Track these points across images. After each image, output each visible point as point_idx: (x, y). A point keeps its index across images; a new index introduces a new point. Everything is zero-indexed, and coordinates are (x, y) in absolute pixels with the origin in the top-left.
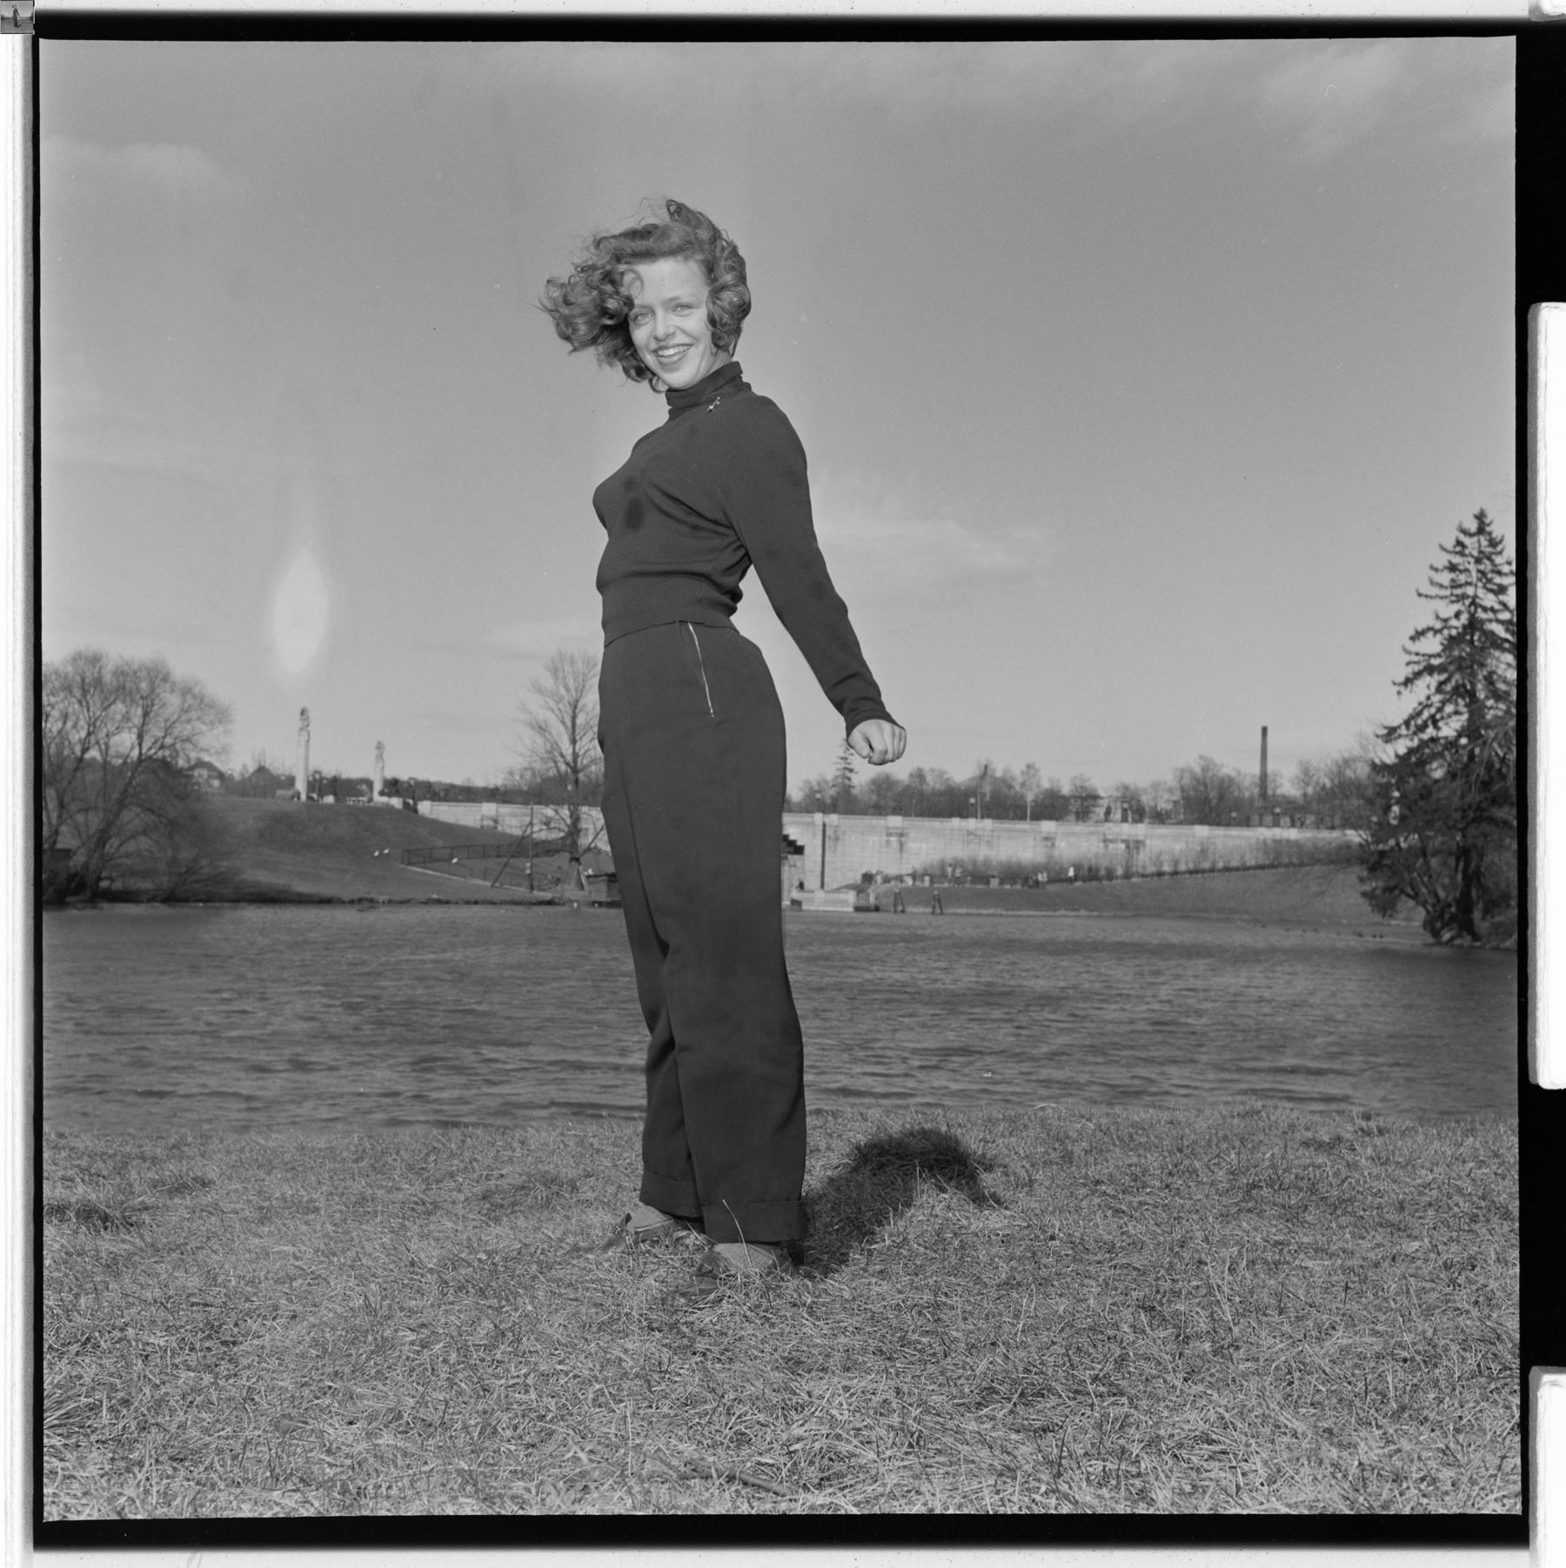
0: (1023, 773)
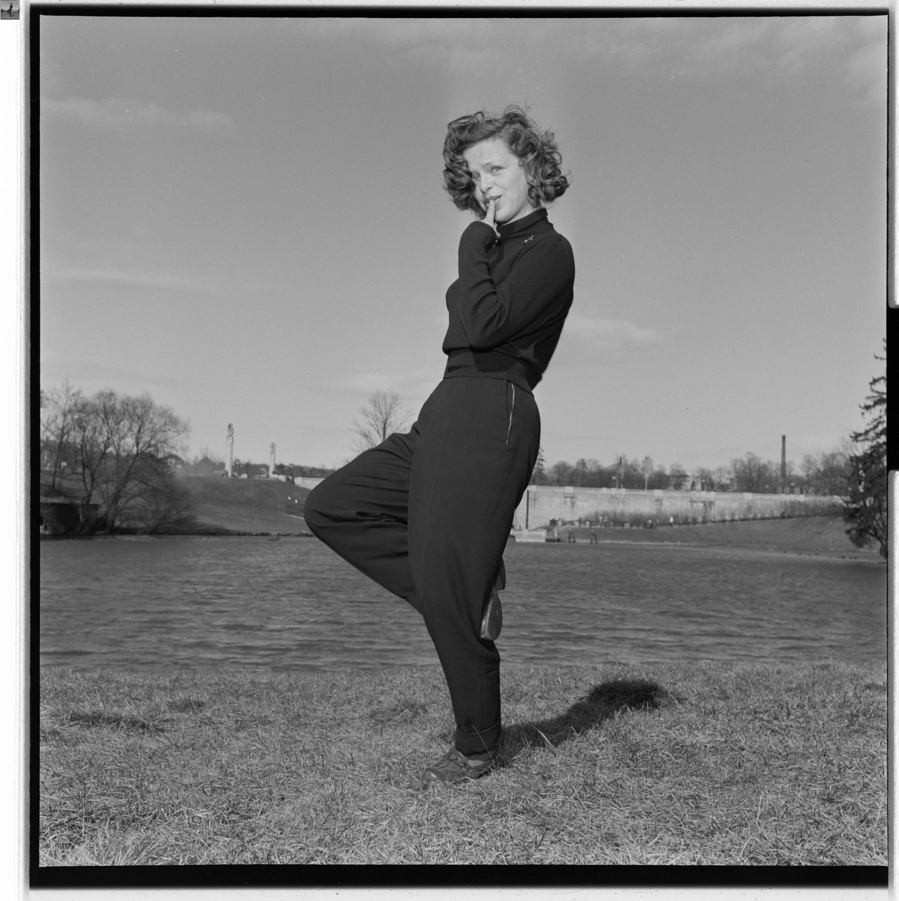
0: (643, 462)
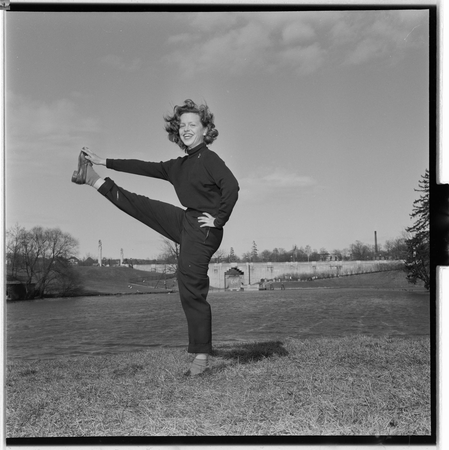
0: (306, 248)
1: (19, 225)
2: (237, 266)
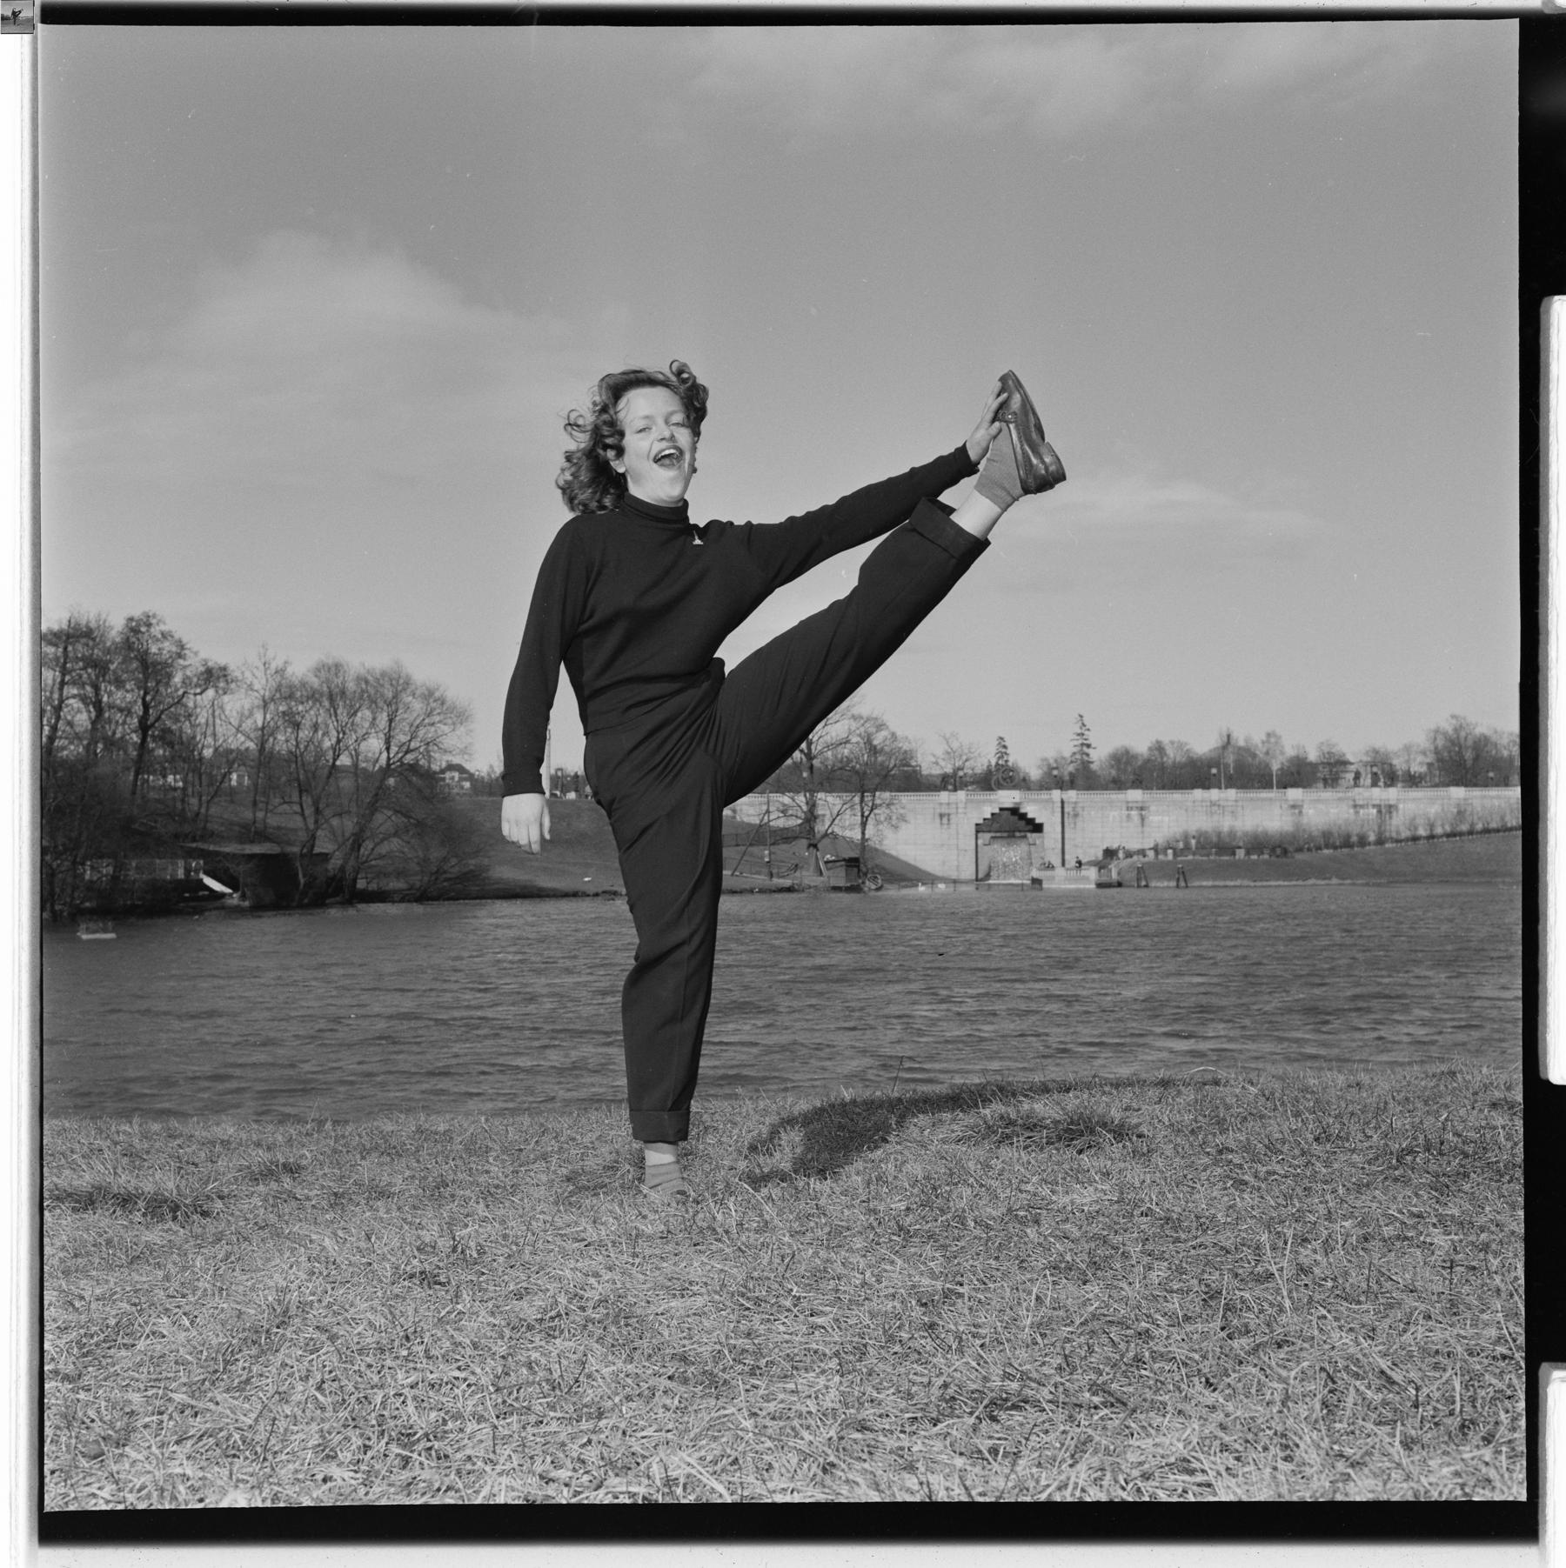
0: (1263, 742)
1: (270, 654)
2: (1020, 803)
